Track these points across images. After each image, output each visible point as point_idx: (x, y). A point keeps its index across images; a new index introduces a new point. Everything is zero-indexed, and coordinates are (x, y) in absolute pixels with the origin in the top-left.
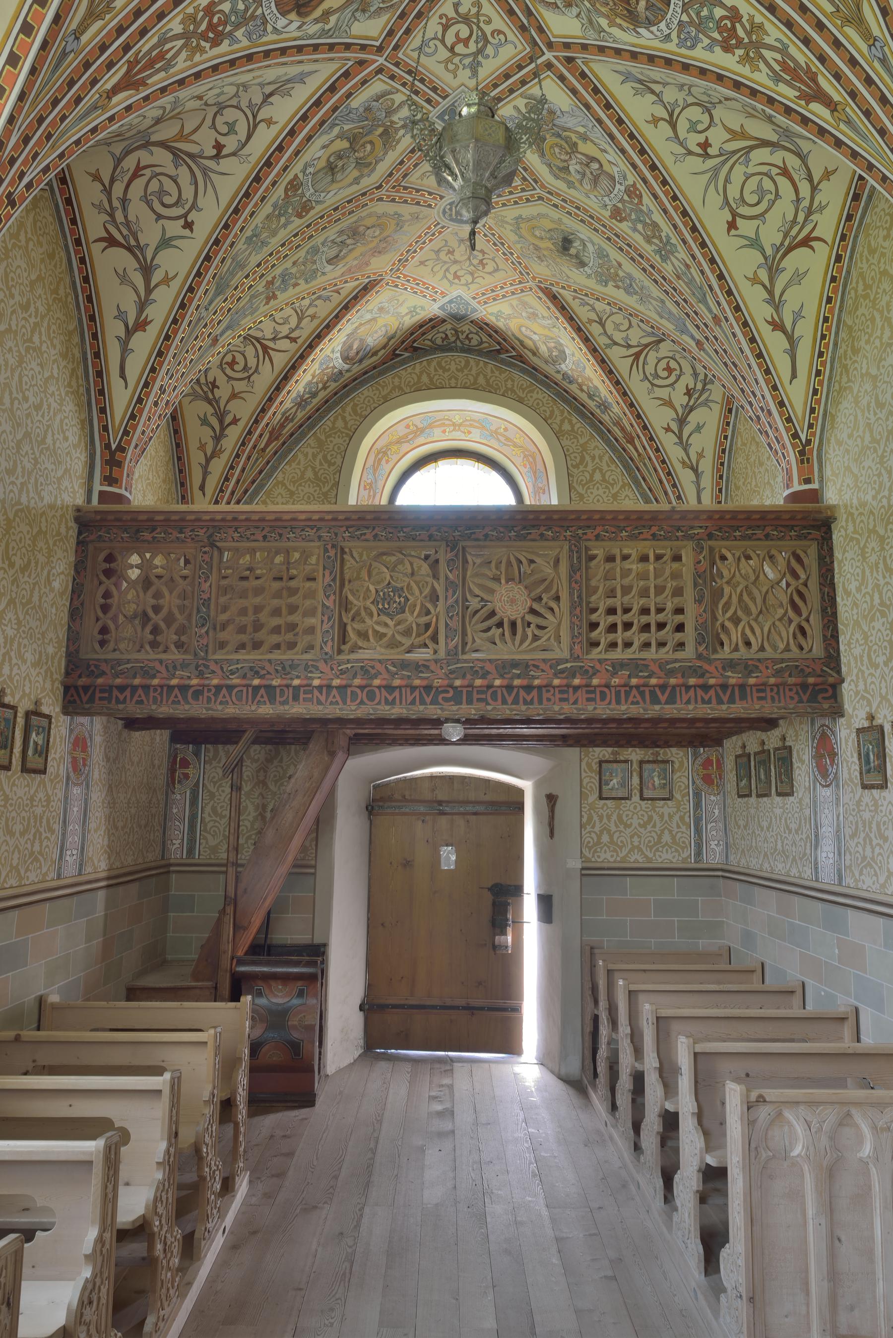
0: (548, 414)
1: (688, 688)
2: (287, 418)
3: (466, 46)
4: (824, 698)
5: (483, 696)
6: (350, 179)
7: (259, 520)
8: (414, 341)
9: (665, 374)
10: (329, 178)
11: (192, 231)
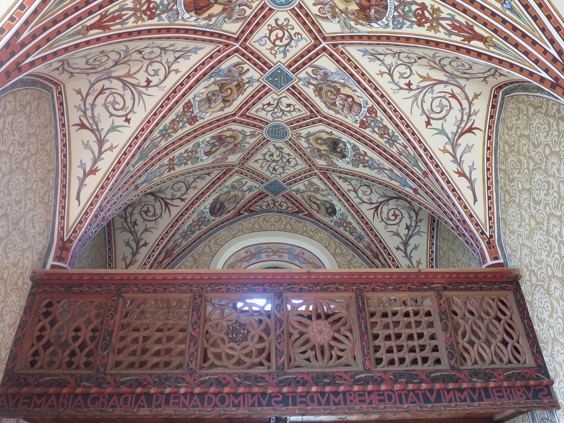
0: (327, 245)
1: (449, 391)
2: (176, 245)
3: (281, 41)
4: (543, 395)
5: (304, 400)
6: (219, 108)
7: (152, 279)
8: (251, 206)
9: (393, 218)
10: (208, 106)
11: (129, 123)
